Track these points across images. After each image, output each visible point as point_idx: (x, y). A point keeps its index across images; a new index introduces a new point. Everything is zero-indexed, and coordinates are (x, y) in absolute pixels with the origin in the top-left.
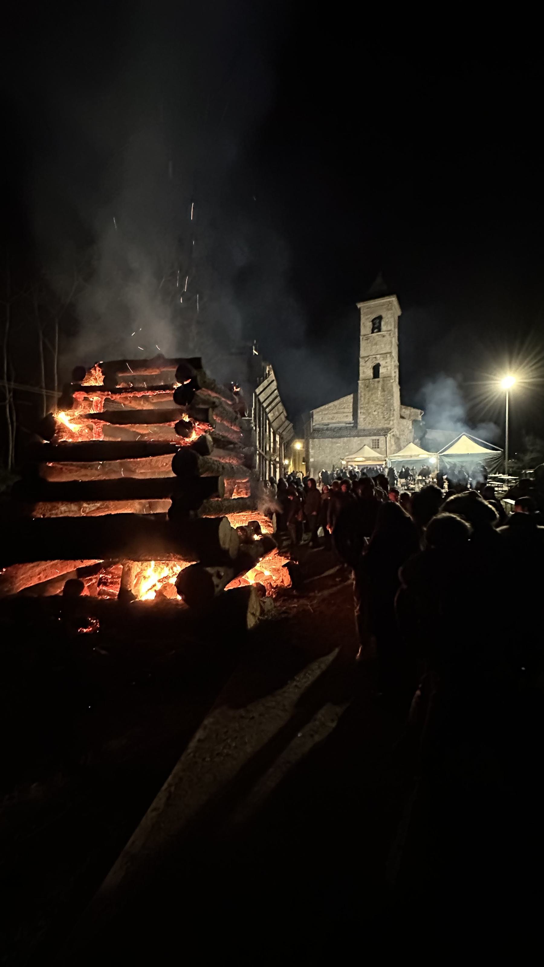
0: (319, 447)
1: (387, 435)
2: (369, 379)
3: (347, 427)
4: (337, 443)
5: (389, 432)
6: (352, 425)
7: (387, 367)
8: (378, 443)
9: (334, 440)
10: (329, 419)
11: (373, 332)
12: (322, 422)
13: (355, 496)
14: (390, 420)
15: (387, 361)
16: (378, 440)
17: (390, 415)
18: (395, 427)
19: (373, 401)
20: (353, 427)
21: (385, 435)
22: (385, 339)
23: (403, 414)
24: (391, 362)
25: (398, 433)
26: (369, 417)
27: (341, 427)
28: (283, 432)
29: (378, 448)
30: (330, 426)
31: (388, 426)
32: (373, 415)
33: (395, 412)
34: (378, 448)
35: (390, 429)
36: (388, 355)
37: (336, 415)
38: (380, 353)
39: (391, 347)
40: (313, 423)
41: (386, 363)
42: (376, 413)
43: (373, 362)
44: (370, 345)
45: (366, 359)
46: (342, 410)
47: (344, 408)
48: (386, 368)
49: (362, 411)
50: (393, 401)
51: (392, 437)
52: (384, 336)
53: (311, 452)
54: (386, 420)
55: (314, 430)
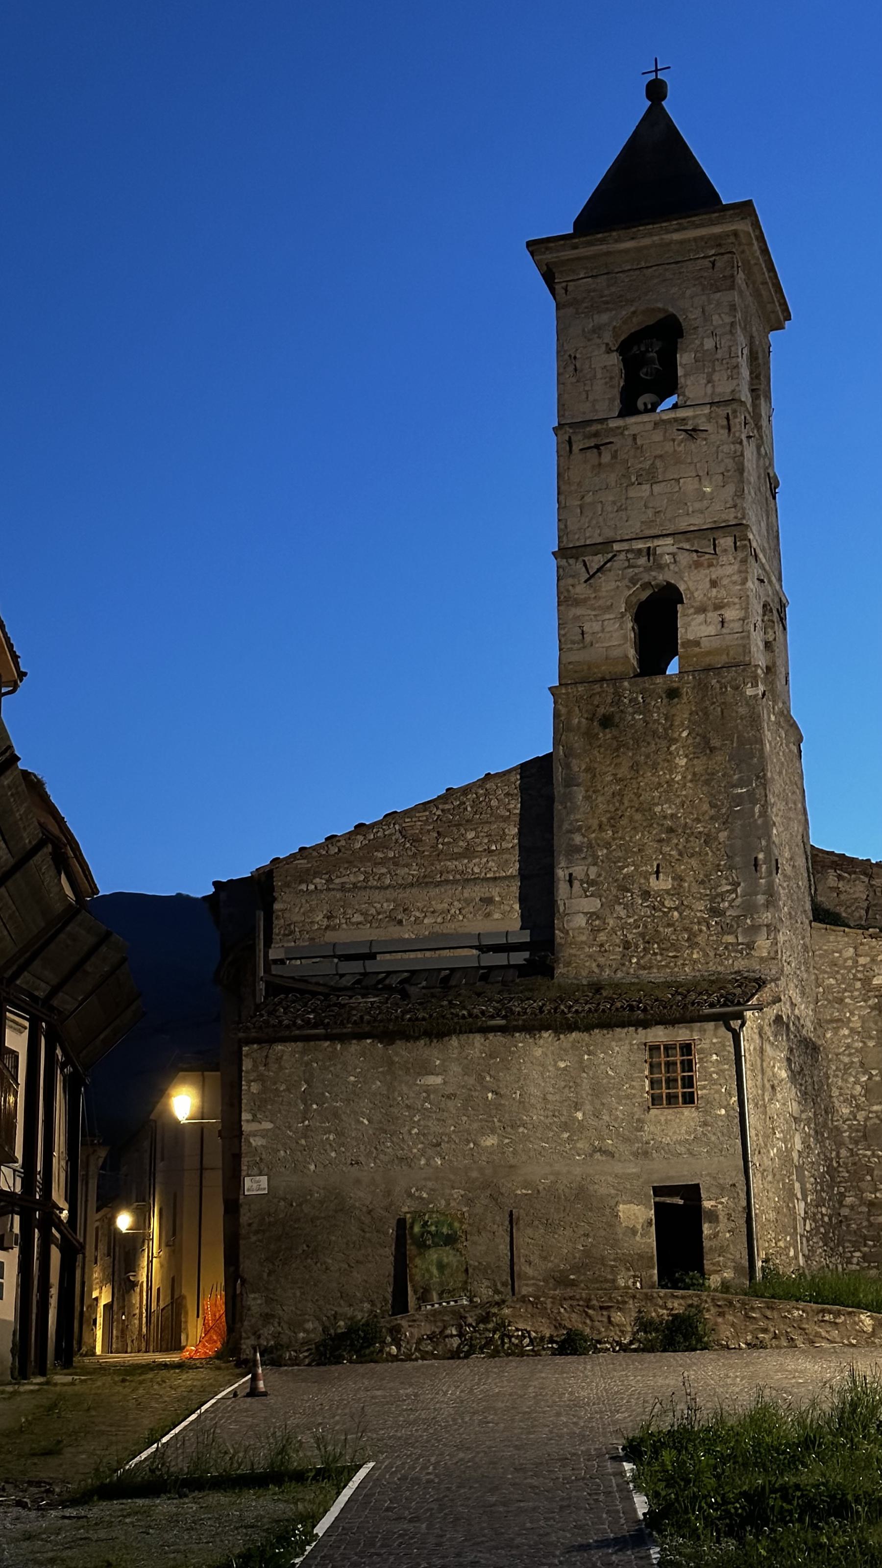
0: (306, 1098)
1: (740, 1016)
2: (615, 679)
3: (487, 974)
4: (426, 1069)
5: (754, 1001)
6: (519, 958)
7: (718, 607)
8: (688, 1066)
9: (402, 1051)
10: (369, 919)
11: (628, 409)
12: (331, 937)
13: (59, 1052)
14: (755, 929)
15: (715, 572)
16: (687, 1049)
17: (751, 893)
18: (787, 969)
19: (645, 809)
20: (522, 970)
21: (724, 1019)
22: (699, 446)
23: (827, 901)
24: (744, 581)
25: (804, 1010)
26: (620, 911)
27: (453, 970)
28: (55, 991)
29: (689, 1099)
30: (384, 962)
31: (741, 964)
32: (646, 894)
33: (778, 879)
34: (689, 1099)
35: (760, 983)
36: (726, 542)
37: (418, 897)
38: (671, 529)
39: (740, 494)
40: (268, 943)
41: (714, 584)
42: (664, 883)
43: (633, 581)
44: (612, 478)
45: (595, 562)
46: (459, 865)
47: (469, 853)
48: (713, 616)
49: (578, 870)
50: (764, 813)
51: (768, 1031)
52: (693, 433)
53: (254, 1134)
54: (726, 929)
55: (274, 989)
